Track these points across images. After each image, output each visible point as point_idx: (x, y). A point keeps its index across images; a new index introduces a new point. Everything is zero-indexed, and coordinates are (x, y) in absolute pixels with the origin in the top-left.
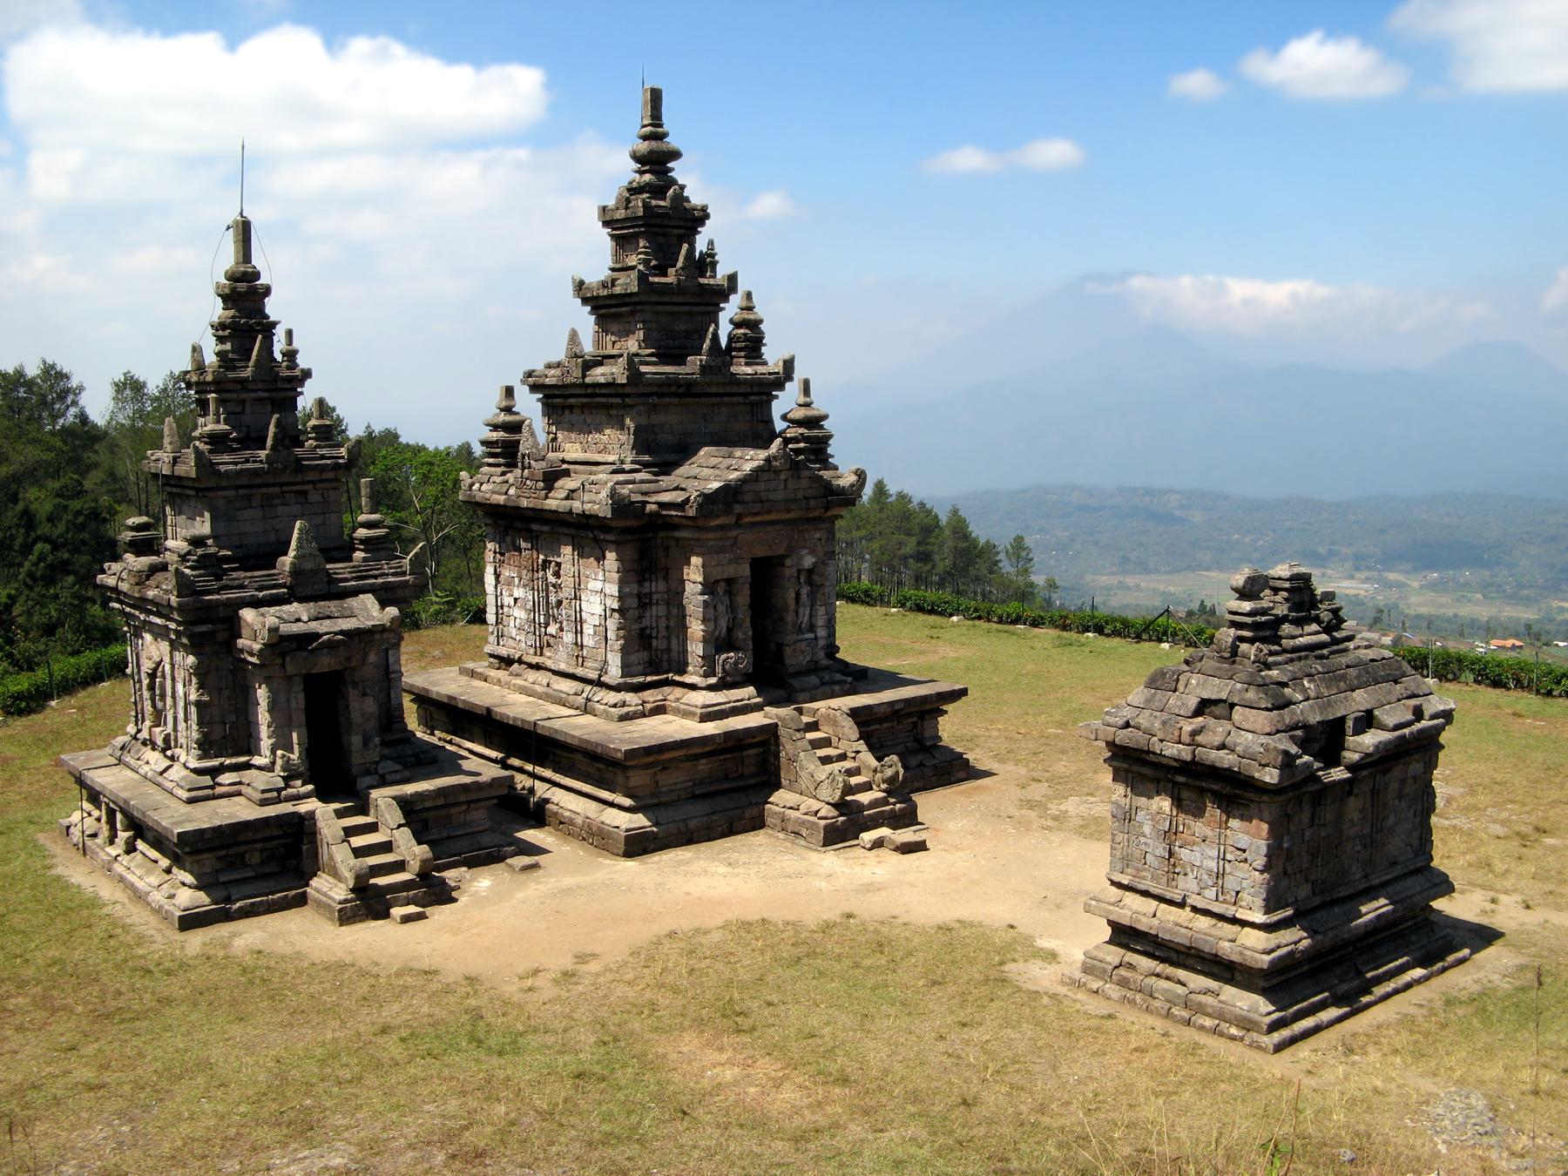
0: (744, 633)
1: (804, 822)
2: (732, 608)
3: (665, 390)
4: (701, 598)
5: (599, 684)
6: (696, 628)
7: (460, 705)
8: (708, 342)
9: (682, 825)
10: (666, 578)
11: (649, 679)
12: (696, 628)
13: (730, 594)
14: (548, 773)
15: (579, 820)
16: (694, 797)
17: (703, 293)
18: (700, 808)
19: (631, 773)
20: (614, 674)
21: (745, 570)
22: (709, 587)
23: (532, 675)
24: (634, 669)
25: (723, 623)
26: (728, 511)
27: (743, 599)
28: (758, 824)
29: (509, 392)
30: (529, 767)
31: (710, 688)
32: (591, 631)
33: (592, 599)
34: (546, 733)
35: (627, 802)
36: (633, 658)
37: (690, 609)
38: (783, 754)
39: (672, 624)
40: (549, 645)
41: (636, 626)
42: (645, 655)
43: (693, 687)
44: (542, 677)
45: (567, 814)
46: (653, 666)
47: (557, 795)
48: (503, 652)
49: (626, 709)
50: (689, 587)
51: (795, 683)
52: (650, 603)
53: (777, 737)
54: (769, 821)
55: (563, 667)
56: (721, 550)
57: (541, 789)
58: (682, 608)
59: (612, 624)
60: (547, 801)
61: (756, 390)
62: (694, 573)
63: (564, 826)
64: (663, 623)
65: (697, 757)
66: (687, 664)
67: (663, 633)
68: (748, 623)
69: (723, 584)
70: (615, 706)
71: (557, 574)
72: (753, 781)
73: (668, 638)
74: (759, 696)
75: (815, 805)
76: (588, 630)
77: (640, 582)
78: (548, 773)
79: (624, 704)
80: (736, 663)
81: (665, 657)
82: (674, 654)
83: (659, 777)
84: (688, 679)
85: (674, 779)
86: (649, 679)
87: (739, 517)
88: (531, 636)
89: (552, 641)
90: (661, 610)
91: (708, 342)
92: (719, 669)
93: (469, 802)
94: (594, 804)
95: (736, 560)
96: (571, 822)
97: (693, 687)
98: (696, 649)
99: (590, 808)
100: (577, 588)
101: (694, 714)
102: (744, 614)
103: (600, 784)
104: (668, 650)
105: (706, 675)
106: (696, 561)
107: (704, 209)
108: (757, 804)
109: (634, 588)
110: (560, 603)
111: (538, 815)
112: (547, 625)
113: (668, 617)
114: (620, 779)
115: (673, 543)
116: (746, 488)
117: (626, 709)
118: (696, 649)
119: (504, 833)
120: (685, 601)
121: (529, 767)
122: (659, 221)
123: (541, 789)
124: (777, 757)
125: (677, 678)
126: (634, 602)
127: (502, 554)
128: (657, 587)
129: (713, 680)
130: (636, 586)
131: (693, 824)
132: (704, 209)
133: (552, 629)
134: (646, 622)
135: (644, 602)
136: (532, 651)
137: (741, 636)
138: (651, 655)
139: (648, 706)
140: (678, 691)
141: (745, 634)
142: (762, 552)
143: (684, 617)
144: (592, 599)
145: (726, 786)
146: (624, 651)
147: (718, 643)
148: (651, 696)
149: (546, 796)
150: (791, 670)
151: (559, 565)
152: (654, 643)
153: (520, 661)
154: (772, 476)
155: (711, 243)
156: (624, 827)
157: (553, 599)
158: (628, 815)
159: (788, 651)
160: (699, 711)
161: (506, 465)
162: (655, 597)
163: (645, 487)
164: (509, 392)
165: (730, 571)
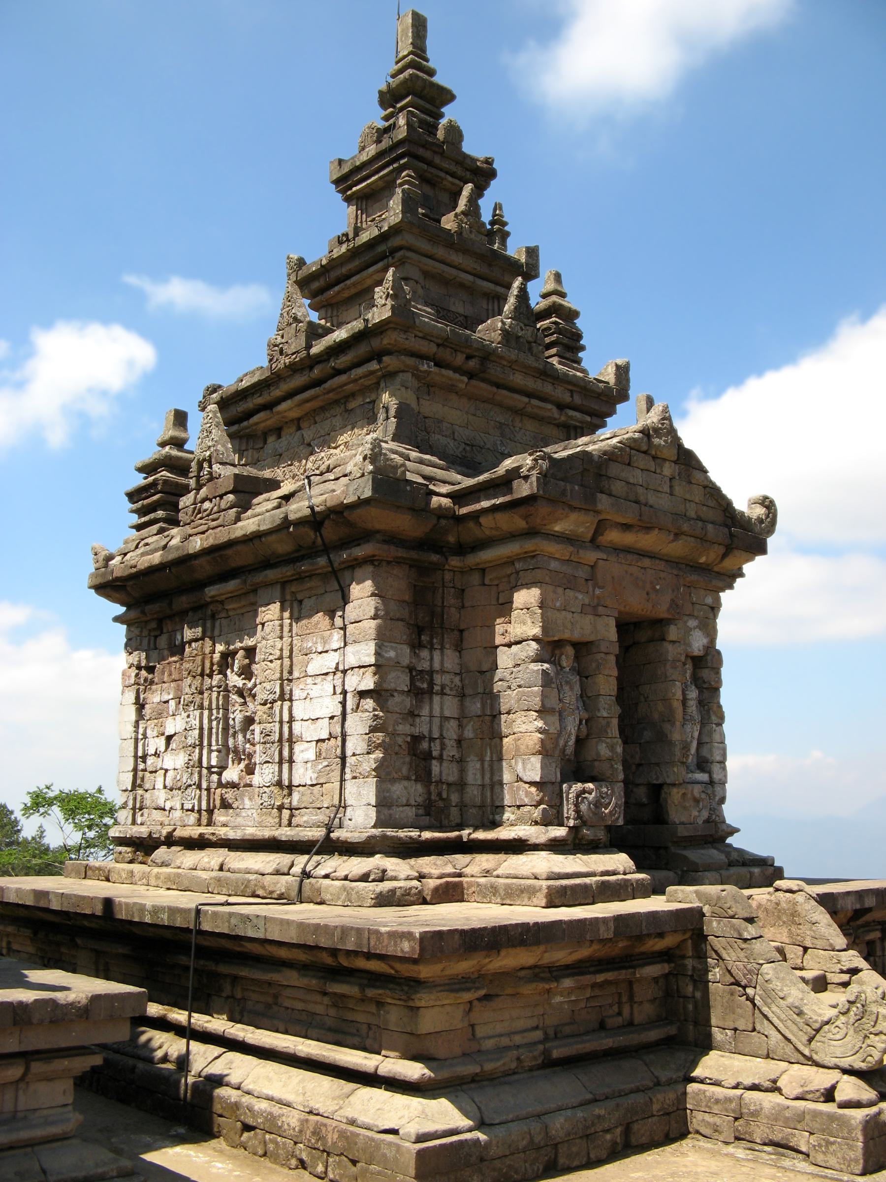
0: (608, 748)
1: (801, 1116)
2: (587, 699)
3: (446, 354)
4: (537, 667)
5: (331, 847)
6: (524, 727)
7: (55, 906)
8: (512, 300)
9: (535, 1127)
10: (459, 648)
11: (427, 835)
12: (524, 727)
13: (583, 674)
14: (218, 1024)
15: (292, 1119)
16: (550, 1064)
17: (487, 265)
18: (563, 1089)
19: (423, 999)
20: (361, 820)
21: (607, 631)
22: (550, 647)
23: (190, 858)
24: (399, 813)
25: (572, 727)
26: (588, 505)
27: (606, 683)
28: (673, 1129)
29: (180, 418)
30: (179, 1016)
31: (555, 846)
32: (311, 755)
33: (315, 691)
34: (223, 928)
35: (414, 1070)
36: (398, 790)
37: (508, 699)
38: (716, 973)
39: (469, 733)
40: (226, 805)
41: (404, 728)
42: (417, 791)
43: (518, 847)
44: (211, 858)
45: (262, 1105)
46: (432, 812)
47: (239, 1068)
48: (141, 831)
49: (387, 886)
50: (505, 658)
51: (694, 855)
52: (430, 692)
53: (700, 937)
54: (697, 1120)
55: (251, 831)
56: (569, 584)
57: (204, 1059)
58: (492, 698)
59: (358, 725)
60: (218, 1081)
61: (578, 400)
62: (523, 620)
63: (254, 1133)
64: (451, 731)
65: (555, 972)
66: (500, 808)
67: (451, 751)
68: (614, 730)
69: (570, 651)
70: (364, 878)
71: (246, 672)
72: (654, 1035)
73: (461, 761)
74: (640, 868)
75: (822, 1079)
76: (304, 752)
77: (416, 646)
78: (218, 1024)
79: (383, 876)
80: (598, 804)
81: (454, 798)
82: (473, 793)
83: (475, 1017)
84: (504, 833)
85: (508, 1023)
86: (427, 835)
87: (601, 527)
88: (193, 792)
89: (230, 795)
90: (449, 706)
91: (512, 300)
92: (568, 810)
93: (26, 1056)
94: (325, 1083)
95: (594, 609)
96: (272, 1126)
97: (518, 847)
98: (523, 765)
99: (321, 1091)
100: (287, 679)
101: (531, 892)
102: (608, 710)
103: (338, 1036)
104: (461, 785)
105: (546, 822)
106: (526, 597)
107: (489, 162)
108: (670, 1083)
109: (401, 653)
110: (249, 721)
111: (194, 1113)
112: (223, 768)
113: (461, 720)
114: (394, 1016)
115: (475, 578)
116: (614, 469)
117: (387, 886)
118: (523, 765)
119: (118, 1152)
120: (498, 687)
121: (179, 1016)
122: (428, 154)
123: (204, 1059)
124: (701, 980)
125: (481, 835)
126: (401, 681)
127: (151, 670)
128: (443, 660)
129: (560, 832)
130: (407, 650)
131: (558, 1124)
132: (489, 162)
133: (232, 774)
134: (422, 727)
135: (421, 687)
136: (192, 818)
137: (603, 750)
138: (437, 794)
139: (432, 883)
140: (485, 861)
141: (612, 748)
142: (637, 603)
143: (496, 716)
144: (315, 691)
145: (608, 1042)
146: (382, 773)
147: (570, 763)
148: (435, 867)
149: (216, 1069)
150: (682, 832)
151: (251, 652)
152: (435, 767)
153: (170, 841)
154: (652, 465)
155: (498, 206)
156: (412, 1129)
157: (237, 716)
158: (415, 1103)
159: (675, 795)
160: (544, 884)
161: (164, 520)
162: (438, 679)
163: (429, 471)
164: (180, 418)
165: (582, 627)
